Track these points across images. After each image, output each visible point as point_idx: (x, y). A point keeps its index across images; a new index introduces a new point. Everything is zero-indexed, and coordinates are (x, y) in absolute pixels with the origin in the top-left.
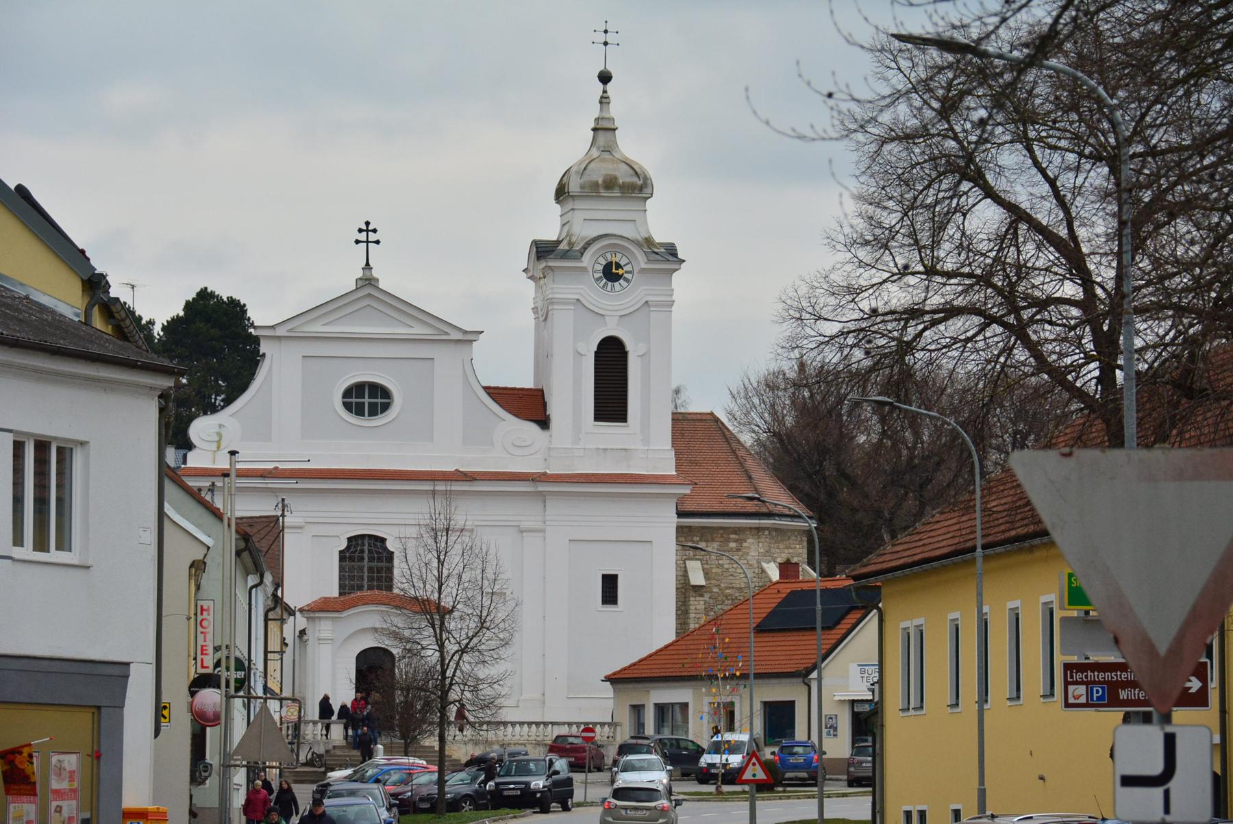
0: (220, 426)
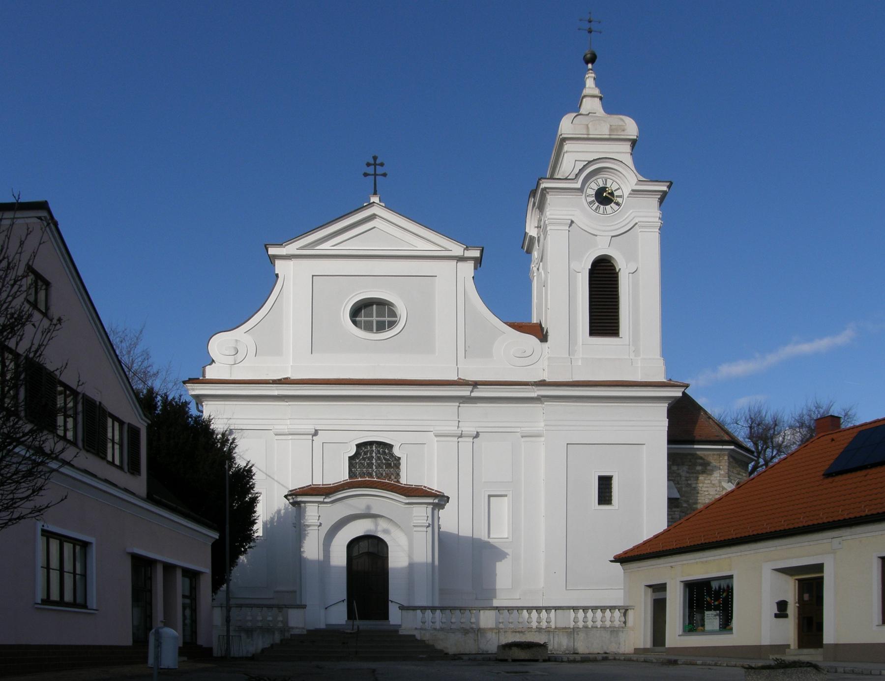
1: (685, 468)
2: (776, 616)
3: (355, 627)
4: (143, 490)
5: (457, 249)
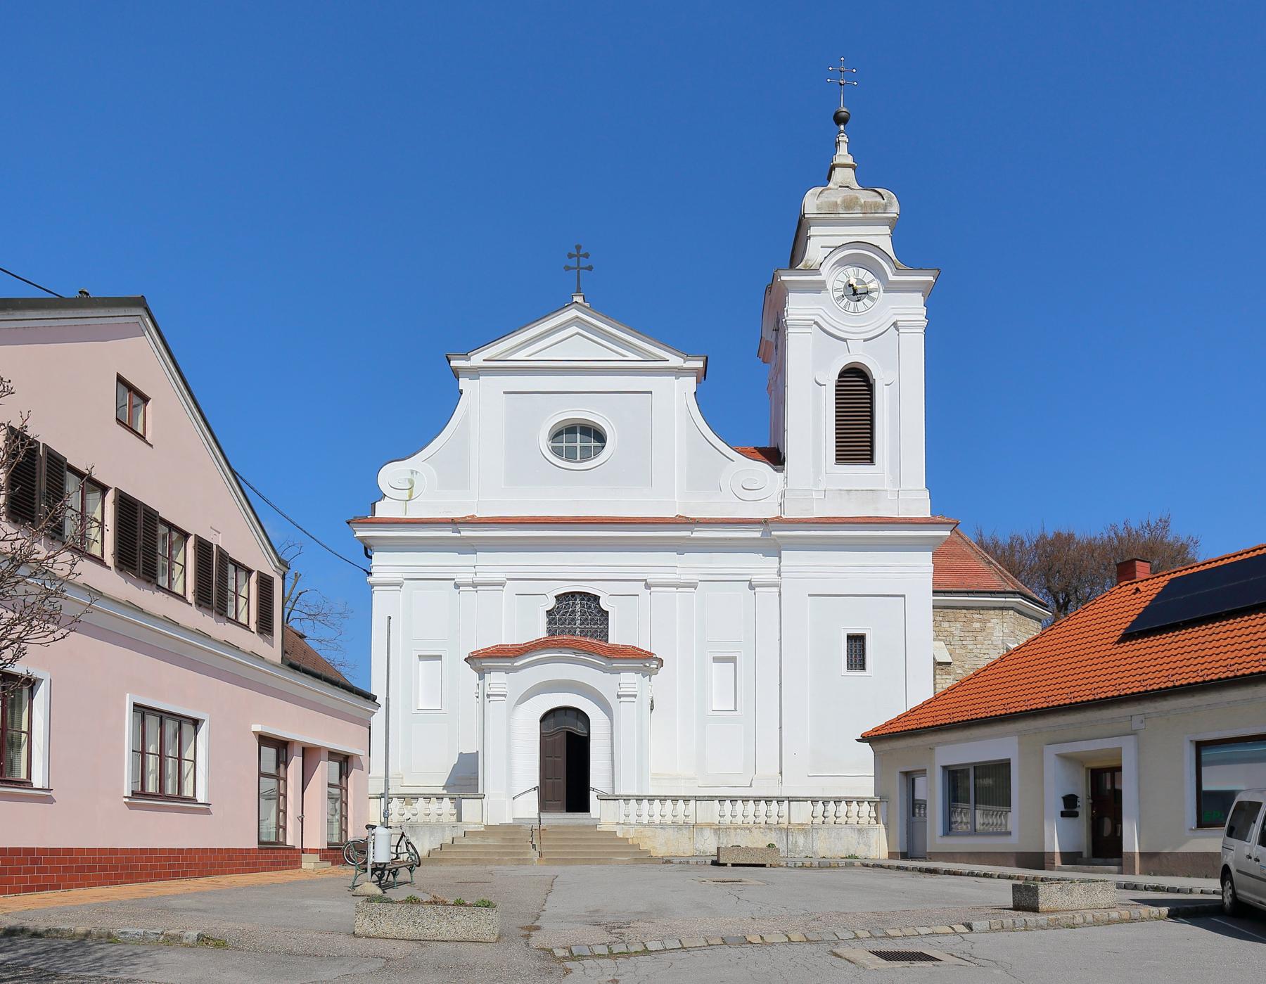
1: (958, 625)
2: (1063, 814)
4: (277, 657)
5: (675, 361)
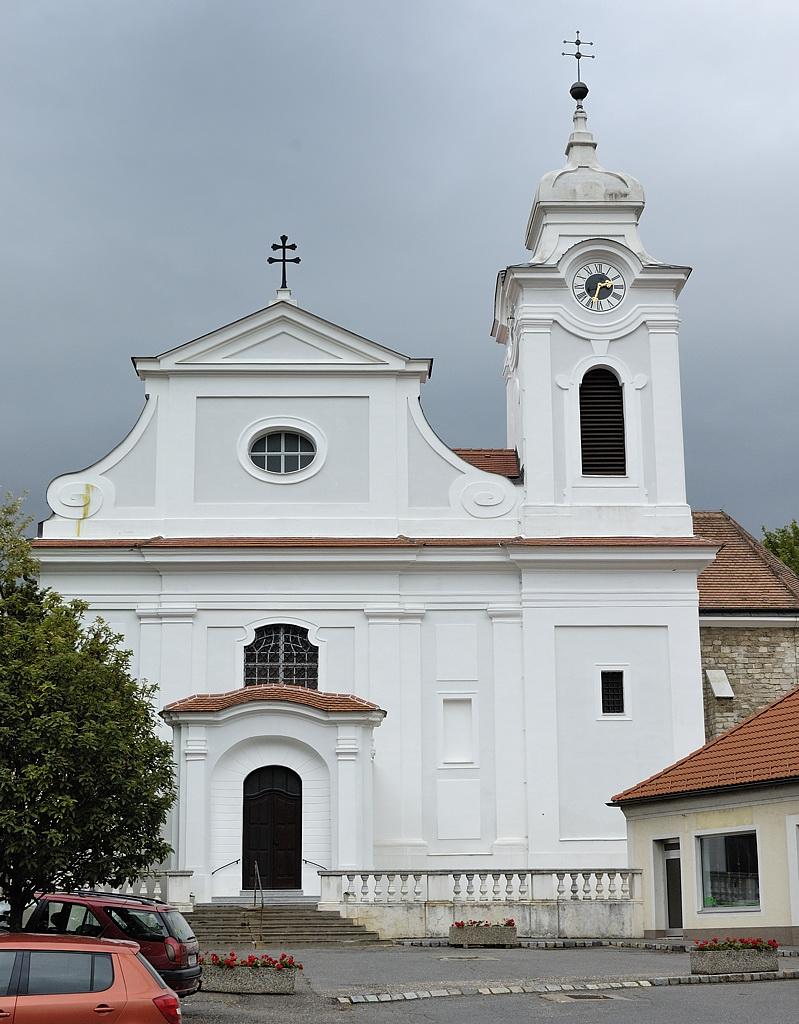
0: (88, 488)
1: (742, 650)
3: (259, 901)
